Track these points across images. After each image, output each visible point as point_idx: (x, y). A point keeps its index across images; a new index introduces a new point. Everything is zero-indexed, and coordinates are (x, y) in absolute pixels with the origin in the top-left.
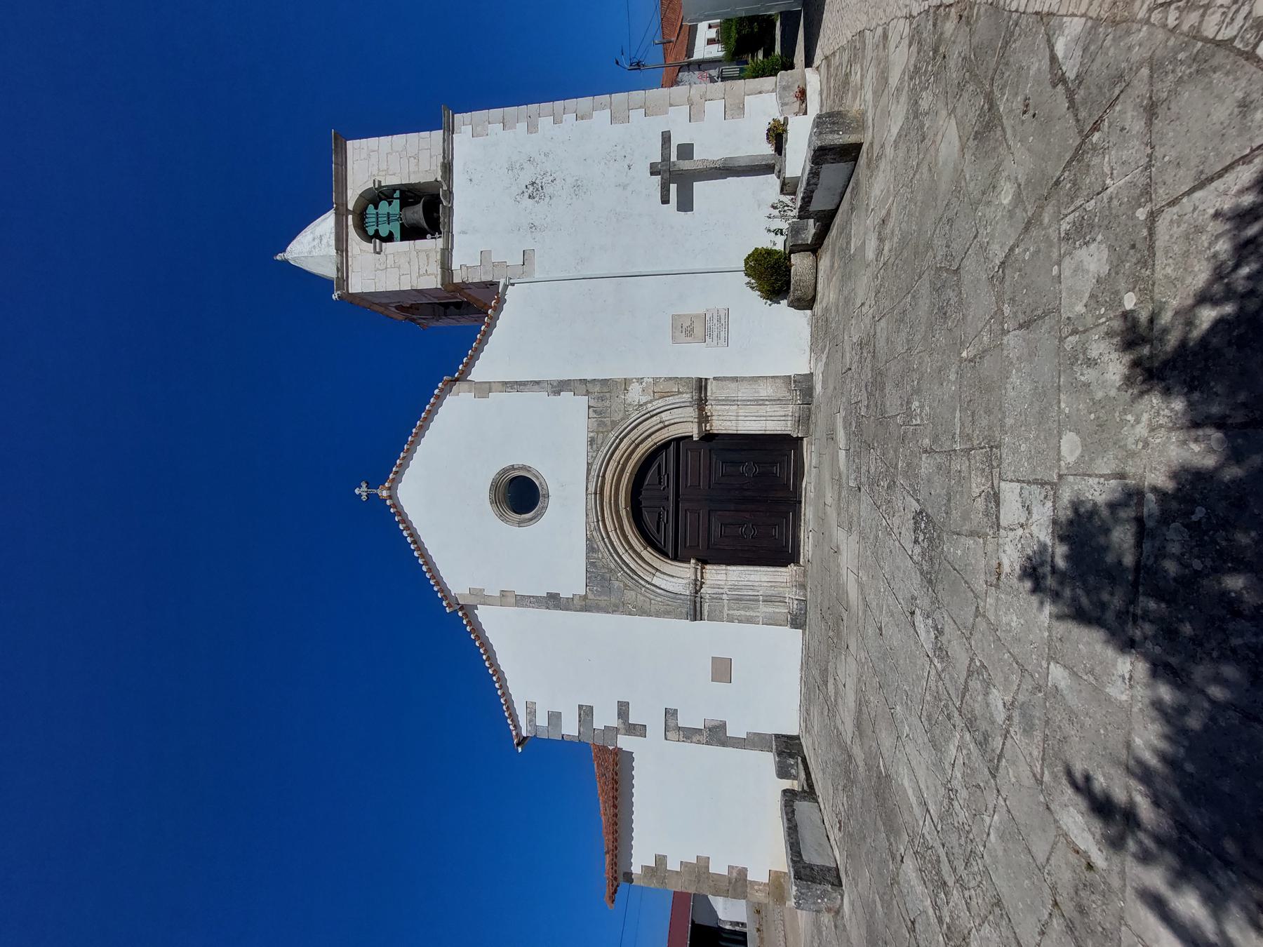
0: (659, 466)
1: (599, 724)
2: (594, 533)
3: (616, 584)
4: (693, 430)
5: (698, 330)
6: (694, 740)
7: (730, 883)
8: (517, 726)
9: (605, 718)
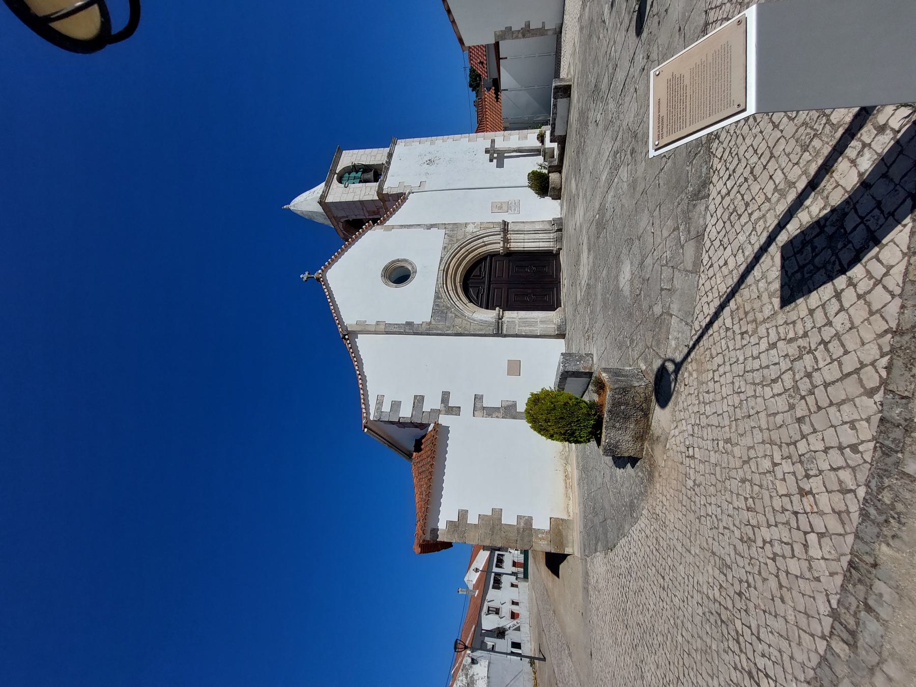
0: (480, 268)
1: (427, 408)
2: (440, 289)
3: (450, 315)
4: (499, 247)
5: (505, 207)
6: (494, 416)
7: (518, 533)
8: (368, 413)
9: (432, 403)
